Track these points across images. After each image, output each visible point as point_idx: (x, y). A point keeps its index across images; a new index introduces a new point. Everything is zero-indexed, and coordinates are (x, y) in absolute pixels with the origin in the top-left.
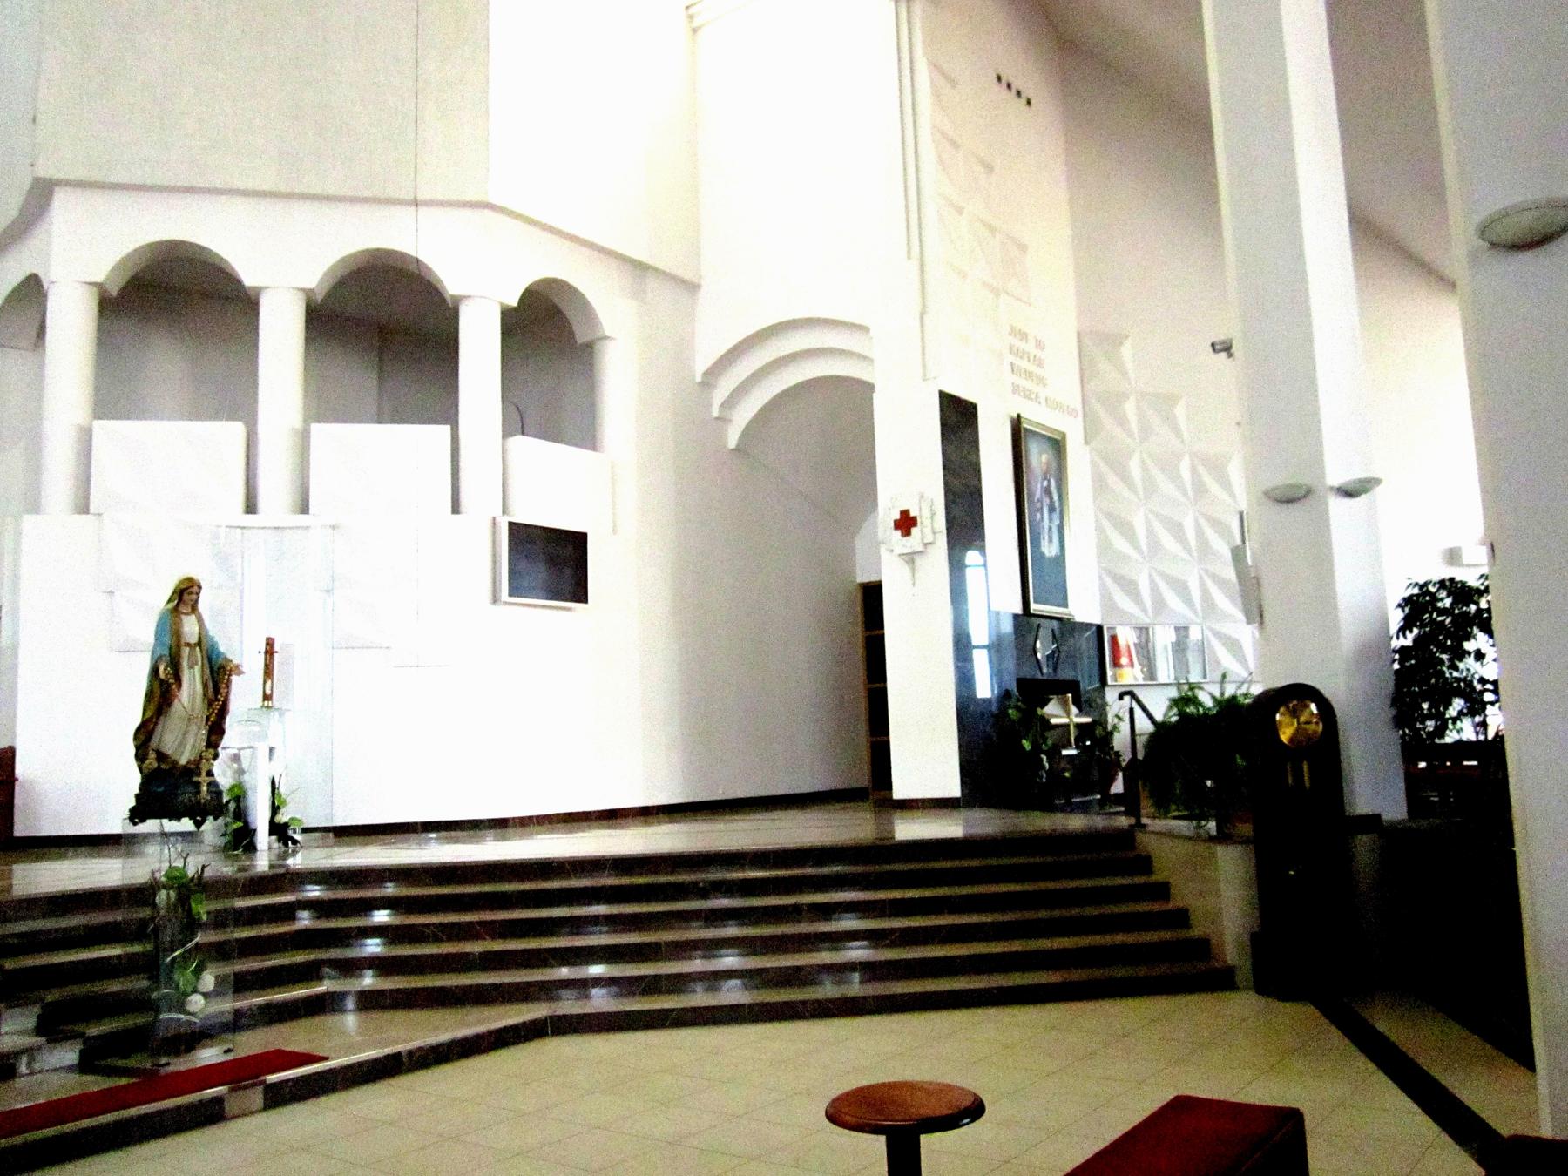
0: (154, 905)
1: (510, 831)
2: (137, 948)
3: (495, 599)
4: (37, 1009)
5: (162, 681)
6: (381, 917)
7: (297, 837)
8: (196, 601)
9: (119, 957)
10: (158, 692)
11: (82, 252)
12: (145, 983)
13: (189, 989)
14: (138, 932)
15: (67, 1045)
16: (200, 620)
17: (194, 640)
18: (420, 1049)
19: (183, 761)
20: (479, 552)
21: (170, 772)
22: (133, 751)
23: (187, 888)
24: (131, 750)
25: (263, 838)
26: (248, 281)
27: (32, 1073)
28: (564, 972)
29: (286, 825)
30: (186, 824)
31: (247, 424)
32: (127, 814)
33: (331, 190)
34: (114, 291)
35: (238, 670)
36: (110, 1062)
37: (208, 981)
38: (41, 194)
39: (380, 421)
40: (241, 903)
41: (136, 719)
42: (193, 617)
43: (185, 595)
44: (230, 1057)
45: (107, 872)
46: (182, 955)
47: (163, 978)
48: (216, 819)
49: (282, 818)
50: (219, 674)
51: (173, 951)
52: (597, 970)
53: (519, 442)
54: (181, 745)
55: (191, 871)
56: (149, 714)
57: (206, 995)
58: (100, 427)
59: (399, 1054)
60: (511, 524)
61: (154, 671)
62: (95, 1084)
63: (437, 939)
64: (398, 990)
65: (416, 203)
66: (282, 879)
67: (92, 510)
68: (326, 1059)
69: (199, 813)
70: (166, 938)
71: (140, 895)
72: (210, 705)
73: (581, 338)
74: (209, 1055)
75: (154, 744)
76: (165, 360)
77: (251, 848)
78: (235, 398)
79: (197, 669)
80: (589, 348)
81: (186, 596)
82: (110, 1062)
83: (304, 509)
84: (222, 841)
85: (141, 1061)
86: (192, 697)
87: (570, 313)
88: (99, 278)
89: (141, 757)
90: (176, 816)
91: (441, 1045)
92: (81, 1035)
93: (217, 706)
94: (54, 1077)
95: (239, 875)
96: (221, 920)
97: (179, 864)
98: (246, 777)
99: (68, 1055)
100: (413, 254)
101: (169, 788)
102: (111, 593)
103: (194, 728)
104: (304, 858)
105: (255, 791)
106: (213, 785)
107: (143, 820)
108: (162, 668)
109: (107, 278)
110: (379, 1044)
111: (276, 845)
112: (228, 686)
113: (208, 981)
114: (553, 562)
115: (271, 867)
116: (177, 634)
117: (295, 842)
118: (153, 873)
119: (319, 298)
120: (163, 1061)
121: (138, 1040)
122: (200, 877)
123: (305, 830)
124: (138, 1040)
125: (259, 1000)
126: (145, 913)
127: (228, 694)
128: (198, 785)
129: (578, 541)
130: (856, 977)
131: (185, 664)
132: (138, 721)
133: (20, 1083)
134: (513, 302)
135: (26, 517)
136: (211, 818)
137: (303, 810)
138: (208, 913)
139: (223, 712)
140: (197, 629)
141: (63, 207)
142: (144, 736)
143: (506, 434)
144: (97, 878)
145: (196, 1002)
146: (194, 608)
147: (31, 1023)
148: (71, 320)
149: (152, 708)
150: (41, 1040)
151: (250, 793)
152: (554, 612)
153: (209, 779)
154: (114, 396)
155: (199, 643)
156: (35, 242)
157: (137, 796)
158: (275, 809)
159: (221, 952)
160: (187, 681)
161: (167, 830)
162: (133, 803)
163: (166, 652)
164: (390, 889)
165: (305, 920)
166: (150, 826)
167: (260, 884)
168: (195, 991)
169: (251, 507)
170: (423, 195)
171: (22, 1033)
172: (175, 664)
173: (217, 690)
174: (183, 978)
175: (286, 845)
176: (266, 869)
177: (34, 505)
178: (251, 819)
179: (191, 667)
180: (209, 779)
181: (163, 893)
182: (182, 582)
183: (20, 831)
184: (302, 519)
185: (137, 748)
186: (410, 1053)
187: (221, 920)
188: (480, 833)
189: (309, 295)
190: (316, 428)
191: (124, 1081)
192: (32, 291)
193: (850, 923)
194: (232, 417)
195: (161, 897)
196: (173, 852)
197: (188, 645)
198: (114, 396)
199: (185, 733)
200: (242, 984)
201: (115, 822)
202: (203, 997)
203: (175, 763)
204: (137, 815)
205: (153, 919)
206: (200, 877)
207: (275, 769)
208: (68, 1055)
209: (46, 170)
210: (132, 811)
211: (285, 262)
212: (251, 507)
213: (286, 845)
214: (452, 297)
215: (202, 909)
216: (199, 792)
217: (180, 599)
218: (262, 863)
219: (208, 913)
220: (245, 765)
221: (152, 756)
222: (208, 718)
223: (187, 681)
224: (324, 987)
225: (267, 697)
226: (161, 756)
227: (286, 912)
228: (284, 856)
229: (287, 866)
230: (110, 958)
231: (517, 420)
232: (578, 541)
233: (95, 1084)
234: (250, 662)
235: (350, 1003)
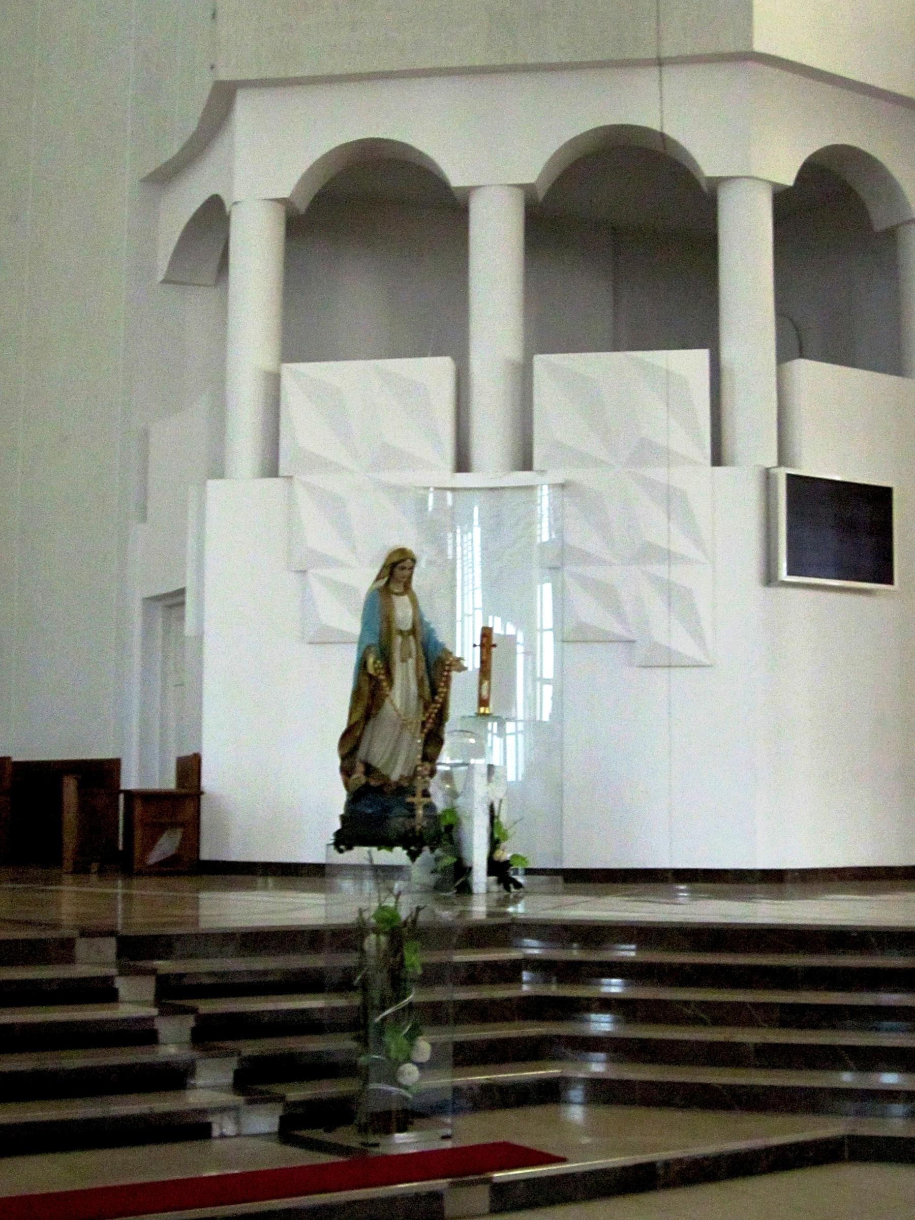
0: (362, 951)
1: (789, 887)
2: (339, 1002)
3: (769, 578)
4: (233, 1064)
5: (370, 676)
6: (614, 987)
7: (520, 879)
8: (410, 578)
9: (321, 1010)
10: (366, 689)
11: (267, 165)
12: (353, 1045)
13: (401, 1058)
14: (344, 985)
15: (264, 1109)
16: (414, 602)
17: (407, 626)
18: (680, 1161)
19: (395, 776)
20: (733, 516)
21: (379, 790)
22: (338, 762)
23: (399, 933)
24: (336, 761)
25: (480, 878)
26: (456, 179)
28: (847, 1079)
29: (507, 864)
30: (398, 856)
31: (455, 359)
32: (331, 839)
33: (554, 57)
34: (302, 206)
35: (458, 665)
36: (304, 1133)
37: (424, 1048)
38: (223, 99)
39: (616, 346)
40: (461, 957)
41: (342, 724)
42: (406, 598)
43: (397, 569)
44: (448, 1144)
45: (305, 909)
46: (395, 1014)
48: (432, 850)
49: (504, 854)
50: (437, 668)
51: (384, 1009)
52: (890, 1079)
53: (807, 371)
54: (394, 755)
55: (404, 913)
56: (356, 718)
57: (420, 1066)
58: (290, 371)
59: (652, 1165)
60: (790, 477)
61: (362, 665)
62: (299, 1157)
63: (695, 1021)
64: (651, 1083)
65: (660, 62)
66: (501, 932)
67: (282, 471)
68: (563, 1160)
69: (413, 842)
70: (375, 994)
71: (345, 937)
72: (426, 708)
73: (880, 220)
74: (405, 1142)
75: (361, 753)
76: (358, 289)
77: (465, 889)
78: (444, 331)
79: (411, 662)
80: (891, 235)
81: (397, 571)
82: (304, 1133)
83: (526, 464)
84: (431, 880)
85: (346, 1136)
86: (406, 701)
87: (863, 190)
88: (286, 193)
89: (346, 771)
90: (388, 844)
91: (706, 1158)
92: (282, 1098)
93: (434, 709)
94: (251, 1142)
95: (458, 922)
96: (433, 976)
97: (390, 903)
98: (460, 801)
99: (264, 1121)
100: (656, 126)
101: (380, 809)
102: (304, 572)
103: (407, 735)
104: (526, 907)
105: (470, 818)
106: (430, 807)
107: (350, 848)
108: (371, 660)
109: (292, 195)
110: (623, 1151)
111: (495, 888)
112: (447, 684)
113: (424, 1048)
114: (847, 527)
115: (490, 914)
116: (388, 619)
117: (518, 885)
118: (361, 911)
119: (541, 194)
120: (372, 1139)
121: (336, 1113)
122: (414, 921)
123: (529, 872)
124: (336, 1113)
125: (480, 1078)
126: (349, 960)
127: (447, 694)
128: (411, 807)
129: (881, 498)
130: (898, 1109)
131: (397, 656)
132: (343, 726)
133: (217, 1145)
134: (788, 179)
135: (211, 483)
136: (426, 849)
137: (528, 848)
138: (424, 966)
139: (441, 716)
140: (410, 612)
141: (246, 112)
142: (351, 745)
143: (784, 355)
144: (297, 915)
145: (410, 1074)
146: (407, 587)
147: (228, 1078)
148: (256, 247)
149: (360, 711)
150: (240, 1100)
151: (464, 821)
152: (832, 596)
153: (425, 800)
154: (303, 338)
155: (413, 631)
156: (217, 154)
157: (343, 818)
158: (494, 844)
159: (435, 1015)
160: (402, 680)
161: (377, 861)
162: (338, 826)
163: (375, 641)
164: (628, 952)
165: (528, 985)
166: (359, 855)
167: (478, 936)
168: (408, 1060)
169: (462, 464)
170: (668, 51)
171: (214, 1088)
172: (385, 656)
173: (434, 692)
174: (394, 1042)
175: (507, 889)
176: (484, 917)
177: (218, 471)
178: (465, 854)
179: (404, 660)
180: (425, 800)
181: (373, 937)
182: (391, 555)
183: (206, 854)
184: (522, 478)
185: (343, 758)
186: (667, 1164)
187: (433, 976)
188: (746, 887)
189: (528, 190)
190: (540, 361)
191: (324, 1159)
192: (213, 218)
194: (437, 352)
195: (371, 942)
196: (375, 890)
197: (401, 632)
198: (303, 338)
199: (398, 740)
200: (465, 1056)
201: (314, 845)
202: (417, 1068)
203: (386, 778)
204: (343, 840)
205: (360, 967)
206: (414, 921)
207: (498, 793)
208: (264, 1121)
209: (224, 75)
210: (338, 834)
211: (495, 152)
212: (462, 464)
213: (507, 889)
214: (710, 179)
215: (415, 959)
216: (413, 816)
217: (391, 574)
218: (479, 909)
219: (424, 966)
220: (459, 788)
221: (360, 768)
222: (424, 724)
223: (402, 680)
224: (551, 1071)
225: (483, 702)
226: (369, 770)
227: (509, 972)
228: (505, 902)
229: (506, 914)
230: (312, 1010)
231: (797, 339)
232: (881, 498)
233: (299, 1157)
234: (472, 659)
235: (577, 1094)
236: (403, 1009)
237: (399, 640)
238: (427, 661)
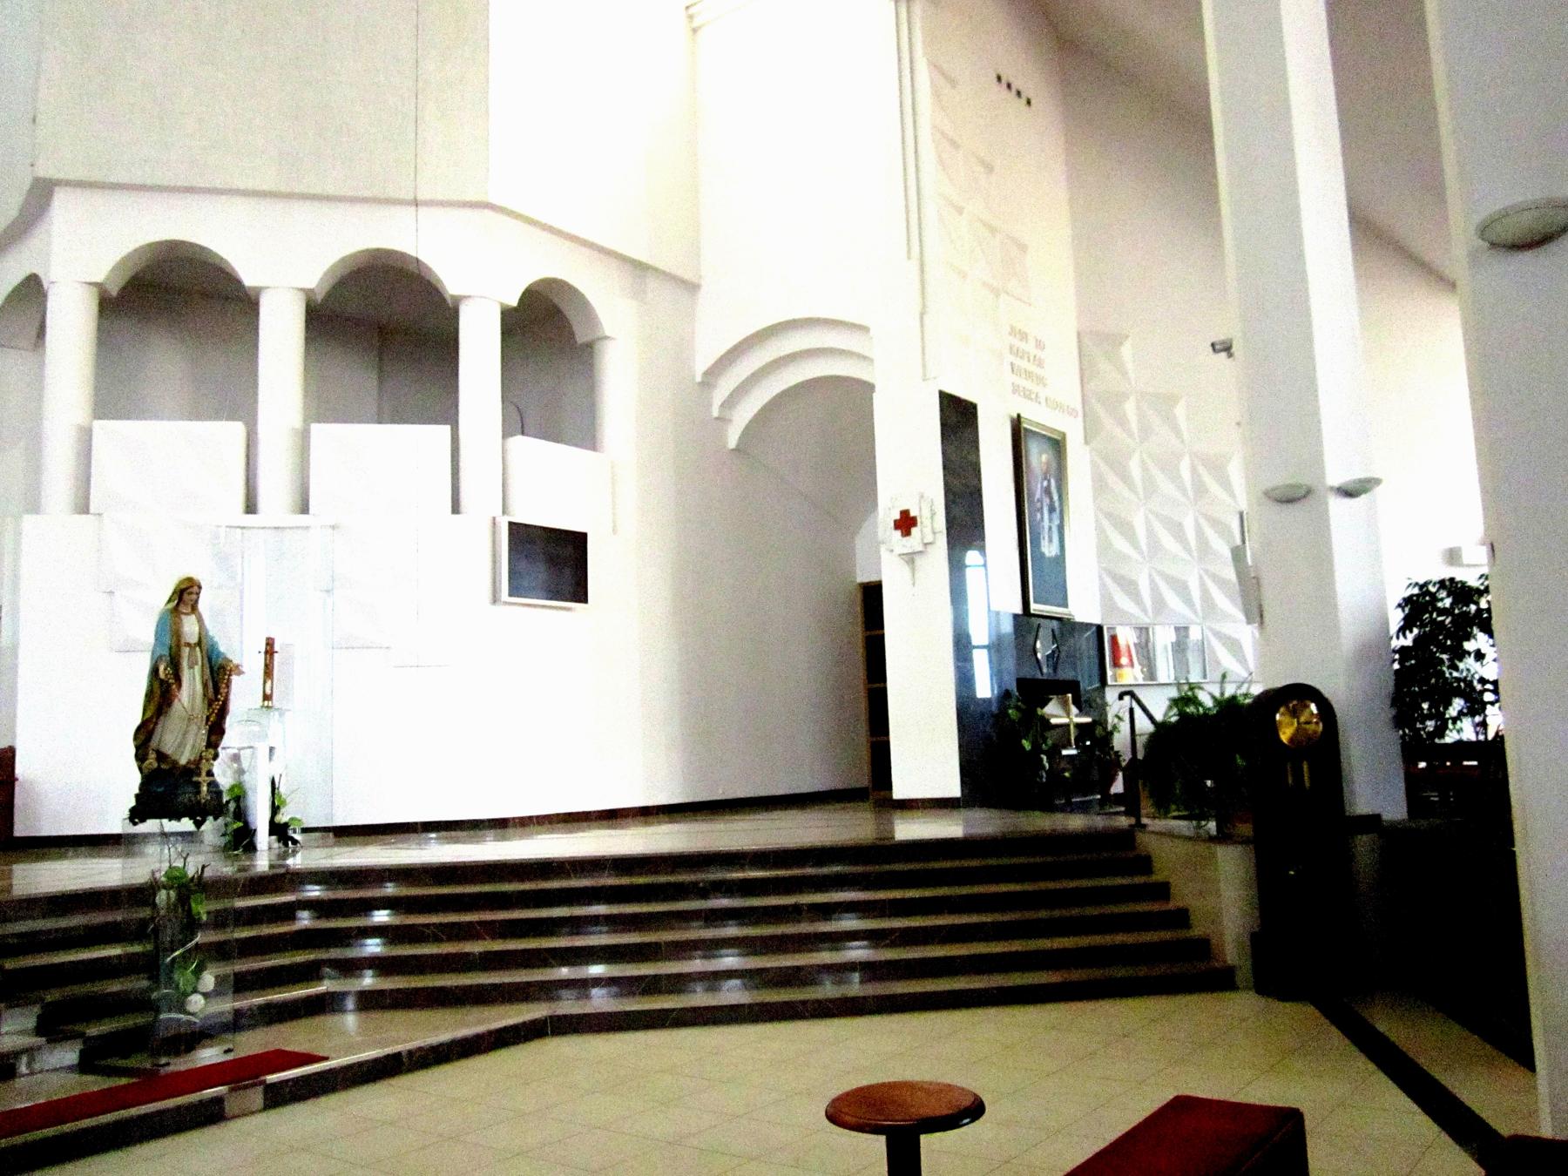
0: (154, 905)
1: (510, 831)
2: (137, 948)
3: (495, 599)
4: (37, 1009)
5: (162, 681)
6: (381, 917)
7: (297, 837)
8: (196, 601)
9: (119, 957)
10: (158, 692)
11: (82, 252)
12: (145, 983)
13: (189, 989)
14: (138, 932)
15: (67, 1045)
16: (200, 620)
17: (194, 640)
18: (420, 1049)
19: (183, 761)
20: (479, 552)
21: (170, 772)
22: (133, 751)
23: (187, 888)
24: (131, 750)
25: (263, 838)
26: (248, 281)
28: (564, 972)
29: (286, 825)
30: (186, 824)
31: (247, 424)
32: (127, 814)
33: (331, 190)
34: (114, 291)
35: (238, 670)
36: (110, 1062)
37: (208, 981)
38: (41, 194)
39: (380, 421)
40: (241, 903)
41: (136, 719)
42: (193, 617)
43: (185, 595)
44: (230, 1057)
45: (107, 872)
46: (182, 955)
48: (216, 819)
49: (282, 818)
50: (219, 674)
51: (173, 951)
52: (597, 970)
53: (519, 442)
54: (181, 745)
55: (191, 871)
56: (149, 714)
57: (206, 995)
58: (100, 427)
59: (399, 1054)
60: (511, 524)
61: (154, 671)
62: (95, 1084)
63: (437, 939)
64: (398, 990)
65: (416, 203)
66: (282, 879)
67: (92, 510)
68: (326, 1059)
69: (199, 813)
70: (166, 938)
71: (140, 895)
72: (210, 705)
73: (581, 338)
74: (209, 1055)
75: (154, 744)
76: (165, 360)
77: (251, 848)
78: (235, 398)
79: (197, 669)
80: (589, 348)
81: (186, 596)
82: (110, 1062)
83: (304, 509)
84: (222, 841)
85: (141, 1061)
86: (192, 697)
87: (570, 313)
88: (99, 278)
89: (141, 757)
90: (176, 816)
91: (441, 1045)
92: (81, 1035)
93: (217, 706)
94: (54, 1077)
95: (239, 875)
96: (221, 920)
97: (179, 864)
98: (246, 777)
99: (68, 1055)
100: (413, 254)
101: (169, 788)
102: (111, 593)
103: (194, 728)
104: (304, 858)
105: (255, 791)
106: (213, 785)
107: (143, 820)
108: (162, 668)
109: (107, 278)
110: (379, 1044)
111: (276, 845)
112: (228, 686)
113: (208, 981)
114: (553, 562)
115: (271, 867)
116: (177, 634)
117: (295, 842)
118: (153, 873)
119: (319, 298)
120: (163, 1061)
121: (138, 1040)
122: (200, 877)
123: (305, 830)
124: (138, 1040)
125: (259, 1000)
126: (145, 913)
127: (228, 694)
128: (198, 785)
129: (578, 541)
131: (185, 664)
132: (138, 721)
133: (20, 1083)
134: (513, 302)
135: (26, 517)
136: (211, 818)
137: (303, 810)
138: (208, 913)
139: (223, 712)
140: (197, 629)
141: (63, 207)
142: (144, 736)
143: (506, 434)
144: (97, 878)
145: (196, 1002)
146: (194, 608)
147: (31, 1023)
148: (71, 320)
149: (152, 708)
150: (41, 1040)
151: (250, 793)
152: (554, 612)
153: (209, 779)
154: (114, 396)
155: (199, 643)
156: (35, 242)
157: (137, 796)
158: (275, 809)
159: (221, 952)
160: (187, 681)
161: (167, 830)
162: (133, 803)
163: (166, 652)
164: (390, 889)
165: (305, 920)
166: (150, 826)
167: (260, 884)
168: (195, 991)
169: (251, 507)
170: (423, 195)
171: (22, 1033)
172: (175, 664)
173: (217, 690)
174: (183, 978)
175: (286, 845)
176: (266, 869)
177: (34, 505)
178: (251, 819)
179: (191, 667)
180: (209, 779)
181: (163, 893)
182: (182, 582)
183: (20, 831)
184: (302, 519)
185: (137, 748)
186: (410, 1053)
187: (221, 920)
188: (480, 833)
189: (309, 295)
190: (316, 428)
191: (124, 1081)
192: (32, 291)
194: (232, 417)
195: (161, 897)
196: (173, 852)
197: (188, 645)
198: (114, 396)
199: (185, 733)
200: (242, 984)
201: (115, 822)
202: (203, 997)
203: (175, 763)
204: (137, 815)
205: (153, 919)
206: (200, 877)
207: (275, 769)
208: (68, 1055)
209: (46, 170)
210: (132, 811)
211: (285, 262)
212: (251, 507)
213: (286, 845)
214: (452, 297)
215: (202, 909)
216: (199, 792)
217: (180, 599)
218: (262, 863)
219: (208, 913)
220: (245, 765)
221: (152, 756)
222: (208, 718)
223: (187, 681)
224: (324, 987)
225: (267, 697)
226: (161, 756)
227: (286, 912)
228: (284, 856)
229: (287, 866)
230: (110, 958)
231: (517, 420)
232: (578, 541)
233: (95, 1084)
234: (250, 662)
235: (350, 1003)
236: (189, 951)
237: (186, 651)
238: (211, 668)
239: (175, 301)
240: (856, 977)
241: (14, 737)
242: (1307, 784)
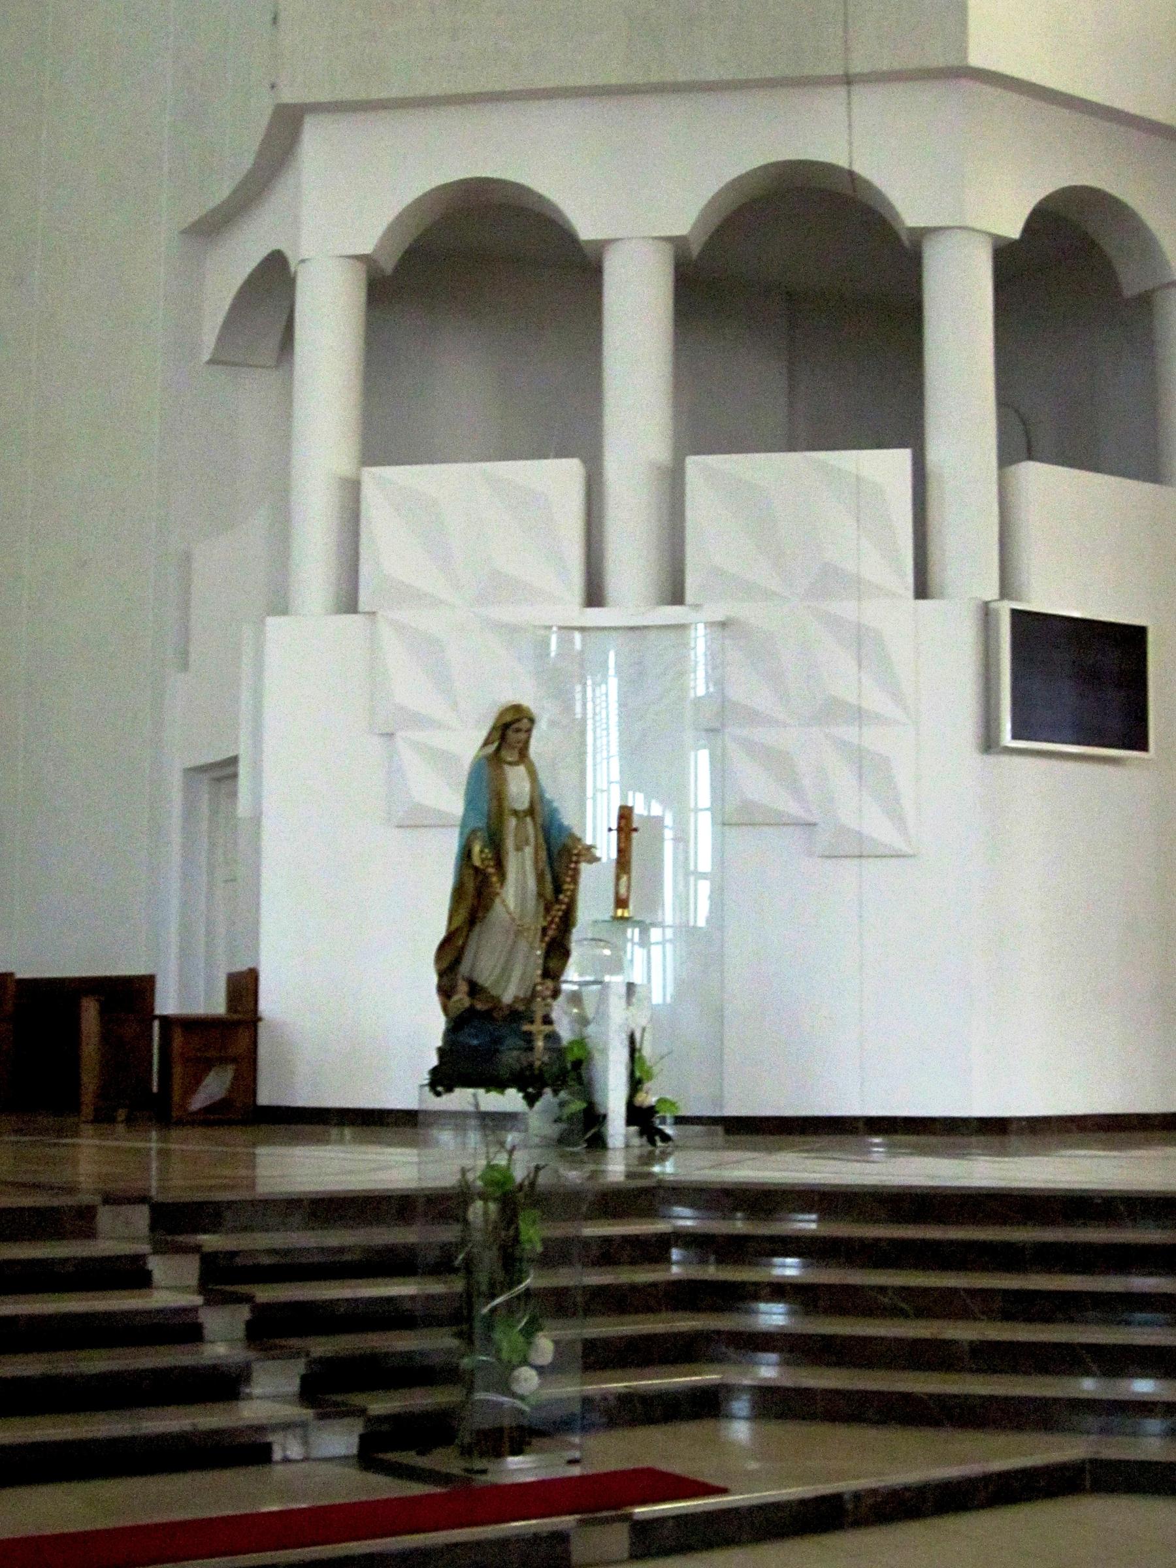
0: (466, 1222)
1: (1014, 1140)
2: (436, 1288)
3: (989, 743)
4: (299, 1367)
5: (476, 869)
6: (789, 1268)
7: (669, 1130)
8: (527, 743)
9: (412, 1298)
10: (470, 885)
11: (343, 212)
12: (454, 1343)
13: (515, 1360)
14: (442, 1267)
15: (339, 1425)
16: (533, 774)
17: (523, 804)
18: (874, 1492)
19: (507, 998)
20: (942, 663)
21: (487, 1015)
22: (434, 979)
23: (512, 1199)
24: (432, 979)
25: (617, 1128)
26: (586, 230)
27: (306, 1459)
28: (1088, 1386)
29: (651, 1111)
30: (511, 1100)
31: (585, 461)
32: (425, 1078)
33: (712, 74)
34: (388, 265)
35: (588, 854)
36: (391, 1456)
37: (544, 1347)
38: (286, 127)
39: (791, 445)
40: (592, 1230)
41: (439, 931)
42: (521, 769)
43: (510, 732)
44: (576, 1471)
45: (392, 1168)
46: (508, 1303)
47: (477, 1343)
48: (556, 1092)
49: (647, 1098)
50: (561, 858)
51: (493, 1296)
52: (1144, 1387)
53: (1037, 477)
54: (506, 970)
55: (519, 1174)
56: (457, 922)
57: (540, 1370)
58: (373, 477)
59: (837, 1497)
60: (1015, 613)
61: (465, 854)
62: (384, 1487)
63: (894, 1312)
64: (837, 1392)
65: (848, 80)
66: (643, 1197)
67: (363, 605)
68: (723, 1491)
69: (531, 1083)
70: (482, 1278)
71: (443, 1205)
72: (548, 909)
73: (1131, 282)
74: (520, 1468)
75: (464, 968)
76: (461, 371)
77: (598, 1143)
78: (571, 426)
79: (529, 851)
80: (1145, 302)
81: (510, 734)
82: (391, 1456)
83: (676, 596)
84: (553, 1131)
85: (445, 1460)
86: (522, 901)
87: (1109, 244)
88: (367, 248)
89: (445, 991)
90: (499, 1084)
91: (907, 1489)
92: (362, 1412)
93: (558, 911)
94: (323, 1468)
95: (589, 1185)
96: (557, 1254)
97: (502, 1160)
98: (591, 1030)
99: (339, 1440)
100: (843, 163)
101: (489, 1039)
102: (391, 735)
103: (523, 945)
104: (676, 1165)
105: (604, 1051)
106: (552, 1037)
107: (449, 1090)
108: (477, 849)
109: (375, 250)
110: (801, 1480)
111: (636, 1141)
112: (575, 880)
113: (544, 1347)
114: (1089, 677)
115: (630, 1175)
116: (498, 796)
117: (666, 1138)
118: (464, 1171)
119: (695, 250)
120: (479, 1464)
121: (432, 1430)
122: (532, 1184)
123: (680, 1120)
124: (432, 1430)
125: (617, 1385)
126: (448, 1234)
127: (574, 892)
128: (529, 1038)
129: (1132, 640)
131: (510, 843)
132: (441, 933)
133: (279, 1471)
134: (1013, 230)
135: (271, 621)
136: (548, 1092)
137: (678, 1089)
138: (544, 1241)
139: (567, 921)
140: (527, 787)
141: (317, 144)
142: (451, 957)
143: (1007, 456)
144: (381, 1175)
145: (527, 1380)
146: (523, 755)
147: (293, 1386)
148: (329, 318)
149: (463, 914)
150: (308, 1413)
151: (597, 1055)
152: (1070, 766)
153: (547, 1029)
154: (389, 435)
155: (531, 812)
156: (279, 198)
157: (441, 1052)
158: (635, 1084)
159: (559, 1304)
160: (517, 874)
161: (484, 1107)
162: (434, 1061)
163: (481, 824)
164: (807, 1224)
165: (678, 1266)
166: (461, 1099)
167: (614, 1202)
168: (525, 1362)
169: (594, 596)
170: (859, 66)
171: (274, 1398)
172: (495, 843)
173: (558, 890)
174: (507, 1339)
175: (652, 1142)
176: (622, 1178)
177: (280, 605)
178: (597, 1098)
179: (519, 849)
180: (547, 1029)
181: (479, 1204)
182: (502, 714)
183: (265, 1097)
184: (671, 614)
185: (441, 974)
186: (857, 1496)
187: (557, 1254)
188: (959, 1140)
189: (678, 244)
190: (694, 464)
191: (417, 1489)
192: (274, 280)
193: (1144, 1387)
194: (562, 452)
195: (476, 1210)
196: (482, 1144)
197: (515, 813)
198: (389, 435)
199: (512, 952)
200: (598, 1357)
201: (403, 1086)
202: (535, 1373)
203: (496, 1000)
204: (441, 1080)
205: (463, 1243)
206: (532, 1184)
207: (639, 1019)
208: (339, 1440)
209: (288, 96)
210: (434, 1072)
211: (636, 196)
212: (594, 596)
213: (652, 1142)
214: (912, 230)
215: (534, 1233)
216: (530, 1048)
217: (503, 738)
218: (616, 1169)
219: (544, 1241)
220: (590, 1012)
221: (463, 987)
222: (544, 930)
223: (517, 874)
224: (709, 1377)
225: (621, 903)
226: (475, 989)
227: (654, 1250)
228: (649, 1159)
229: (651, 1175)
230: (401, 1298)
231: (1024, 435)
232: (1132, 640)
233: (384, 1487)
234: (606, 847)
235: (741, 1406)
237: (512, 822)
238: (549, 850)
239: (482, 279)
240: (1154, 1425)
241: (255, 948)
242: (155, 1089)
